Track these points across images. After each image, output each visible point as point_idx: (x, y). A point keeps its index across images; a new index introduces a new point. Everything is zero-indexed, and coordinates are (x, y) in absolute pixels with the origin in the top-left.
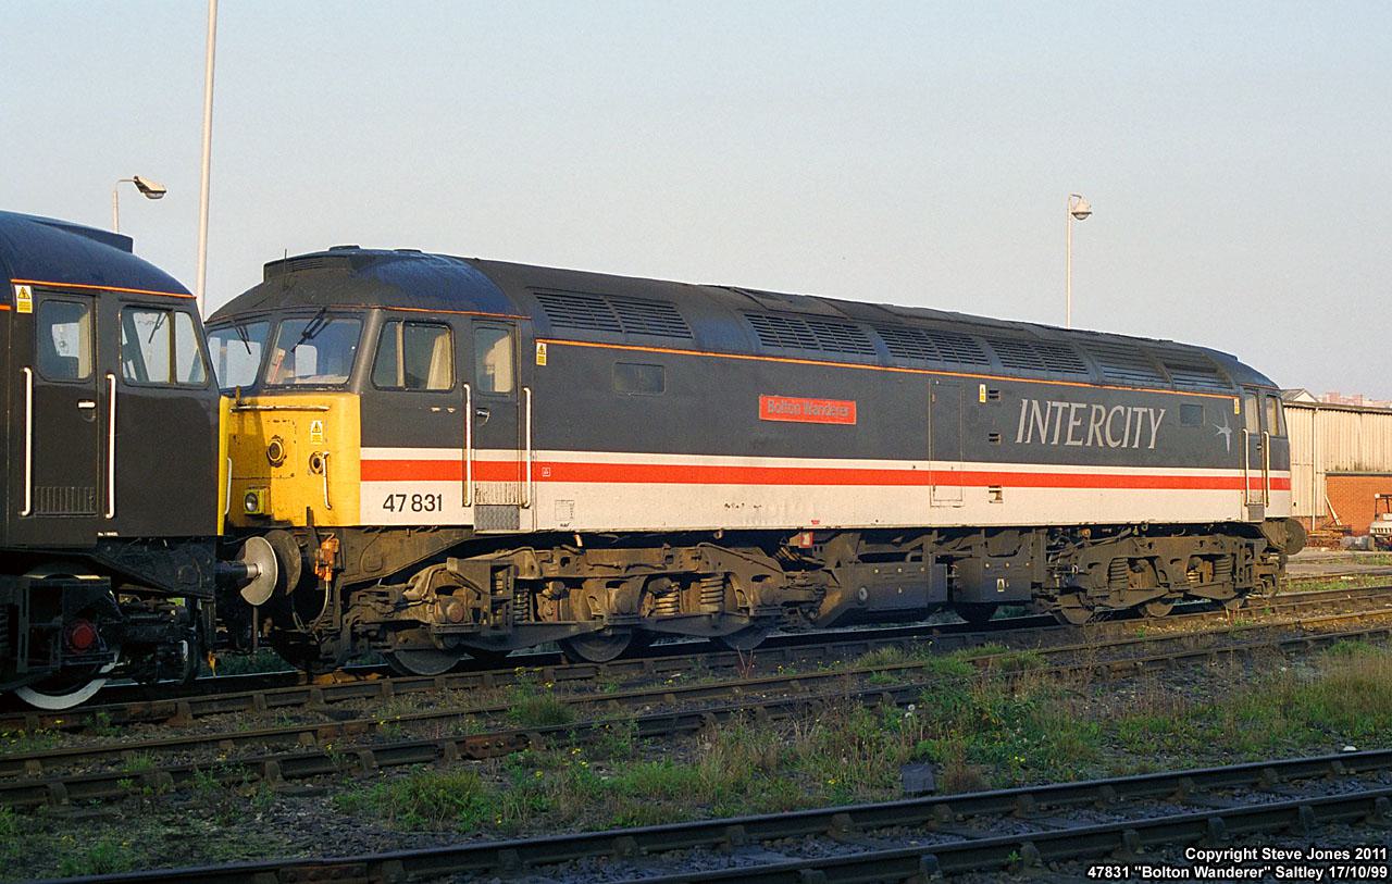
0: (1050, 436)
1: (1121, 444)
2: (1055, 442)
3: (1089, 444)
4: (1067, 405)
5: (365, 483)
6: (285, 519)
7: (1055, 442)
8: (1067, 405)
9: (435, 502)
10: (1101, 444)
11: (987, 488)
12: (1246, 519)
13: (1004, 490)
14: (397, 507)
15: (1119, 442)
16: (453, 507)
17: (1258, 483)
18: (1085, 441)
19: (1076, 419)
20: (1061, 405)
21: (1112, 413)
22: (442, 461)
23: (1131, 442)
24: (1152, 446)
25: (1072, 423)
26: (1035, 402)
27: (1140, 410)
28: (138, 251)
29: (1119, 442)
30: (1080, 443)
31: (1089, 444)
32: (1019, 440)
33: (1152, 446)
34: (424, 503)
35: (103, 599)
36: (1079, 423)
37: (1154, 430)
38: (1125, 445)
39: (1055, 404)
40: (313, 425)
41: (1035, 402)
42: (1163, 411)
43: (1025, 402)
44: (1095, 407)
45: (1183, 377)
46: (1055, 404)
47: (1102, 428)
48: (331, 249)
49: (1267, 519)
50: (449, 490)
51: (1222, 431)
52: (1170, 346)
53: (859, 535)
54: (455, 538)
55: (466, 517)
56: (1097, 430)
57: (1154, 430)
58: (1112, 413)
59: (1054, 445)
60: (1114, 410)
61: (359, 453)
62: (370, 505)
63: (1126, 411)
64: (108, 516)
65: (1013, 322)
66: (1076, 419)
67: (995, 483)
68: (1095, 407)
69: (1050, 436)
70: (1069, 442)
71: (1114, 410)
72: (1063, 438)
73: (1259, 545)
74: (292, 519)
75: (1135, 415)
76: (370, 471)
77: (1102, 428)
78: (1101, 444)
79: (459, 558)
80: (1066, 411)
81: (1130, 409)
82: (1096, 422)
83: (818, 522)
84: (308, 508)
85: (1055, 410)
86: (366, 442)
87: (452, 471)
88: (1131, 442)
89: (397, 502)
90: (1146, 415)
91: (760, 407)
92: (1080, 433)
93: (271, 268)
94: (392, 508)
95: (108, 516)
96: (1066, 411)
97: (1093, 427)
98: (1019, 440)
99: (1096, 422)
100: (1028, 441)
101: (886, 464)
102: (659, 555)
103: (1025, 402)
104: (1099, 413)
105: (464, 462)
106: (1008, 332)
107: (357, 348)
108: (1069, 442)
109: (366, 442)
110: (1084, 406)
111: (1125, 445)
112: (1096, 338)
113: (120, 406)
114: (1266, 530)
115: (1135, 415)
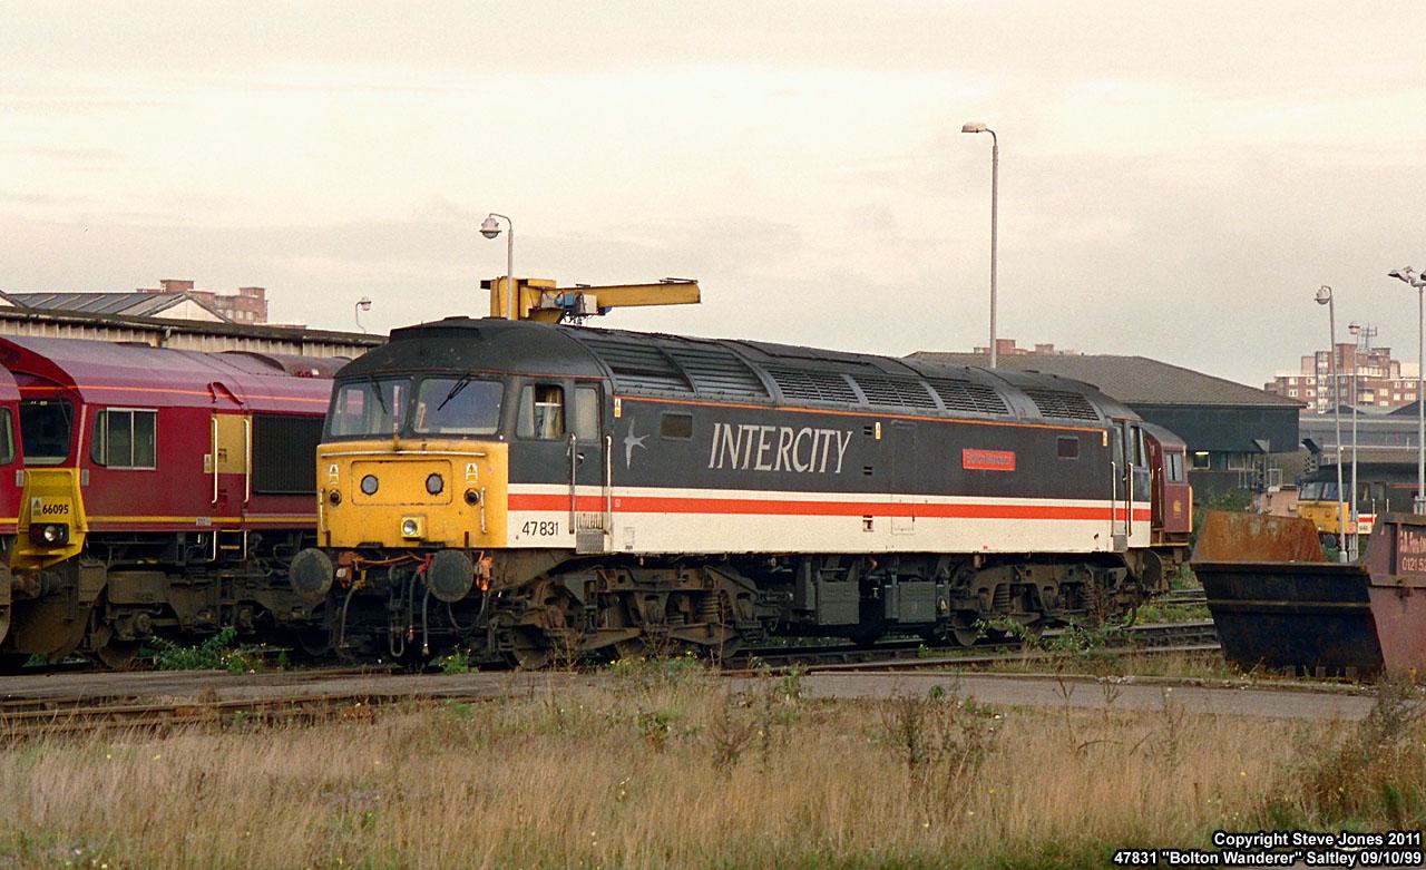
0: (741, 462)
1: (808, 468)
3: (777, 468)
4: (757, 428)
5: (513, 513)
6: (440, 540)
8: (757, 428)
10: (788, 469)
11: (862, 518)
12: (1111, 550)
13: (875, 519)
14: (531, 530)
15: (807, 466)
16: (561, 533)
17: (1109, 514)
18: (774, 467)
19: (765, 443)
20: (751, 428)
21: (799, 436)
22: (871, 504)
24: (838, 471)
25: (762, 447)
26: (727, 427)
27: (828, 433)
28: (1101, 390)
29: (807, 466)
30: (769, 468)
31: (777, 468)
32: (711, 465)
33: (838, 471)
34: (548, 528)
36: (767, 447)
37: (841, 453)
38: (811, 470)
39: (746, 427)
40: (468, 468)
41: (727, 427)
42: (850, 433)
43: (718, 426)
44: (783, 430)
45: (722, 379)
46: (746, 427)
47: (790, 452)
48: (446, 319)
49: (1130, 549)
50: (561, 518)
51: (638, 442)
52: (463, 324)
53: (838, 561)
54: (561, 558)
55: (569, 541)
56: (785, 453)
57: (841, 453)
58: (799, 436)
59: (838, 475)
60: (802, 433)
61: (506, 488)
62: (515, 530)
63: (814, 433)
65: (859, 355)
66: (765, 443)
67: (868, 512)
68: (783, 430)
69: (741, 462)
70: (759, 467)
71: (802, 433)
73: (1120, 573)
74: (384, 541)
75: (822, 437)
76: (516, 503)
77: (790, 452)
78: (788, 469)
80: (756, 434)
81: (817, 431)
82: (784, 446)
83: (631, 547)
84: (467, 534)
85: (745, 433)
87: (568, 503)
89: (532, 527)
92: (769, 457)
96: (756, 434)
97: (783, 450)
98: (711, 465)
99: (784, 446)
100: (720, 466)
101: (649, 492)
102: (1196, 558)
103: (718, 426)
104: (787, 435)
105: (1112, 509)
106: (801, 362)
107: (502, 406)
108: (759, 467)
110: (774, 429)
111: (811, 470)
112: (609, 338)
114: (1130, 561)
115: (822, 437)
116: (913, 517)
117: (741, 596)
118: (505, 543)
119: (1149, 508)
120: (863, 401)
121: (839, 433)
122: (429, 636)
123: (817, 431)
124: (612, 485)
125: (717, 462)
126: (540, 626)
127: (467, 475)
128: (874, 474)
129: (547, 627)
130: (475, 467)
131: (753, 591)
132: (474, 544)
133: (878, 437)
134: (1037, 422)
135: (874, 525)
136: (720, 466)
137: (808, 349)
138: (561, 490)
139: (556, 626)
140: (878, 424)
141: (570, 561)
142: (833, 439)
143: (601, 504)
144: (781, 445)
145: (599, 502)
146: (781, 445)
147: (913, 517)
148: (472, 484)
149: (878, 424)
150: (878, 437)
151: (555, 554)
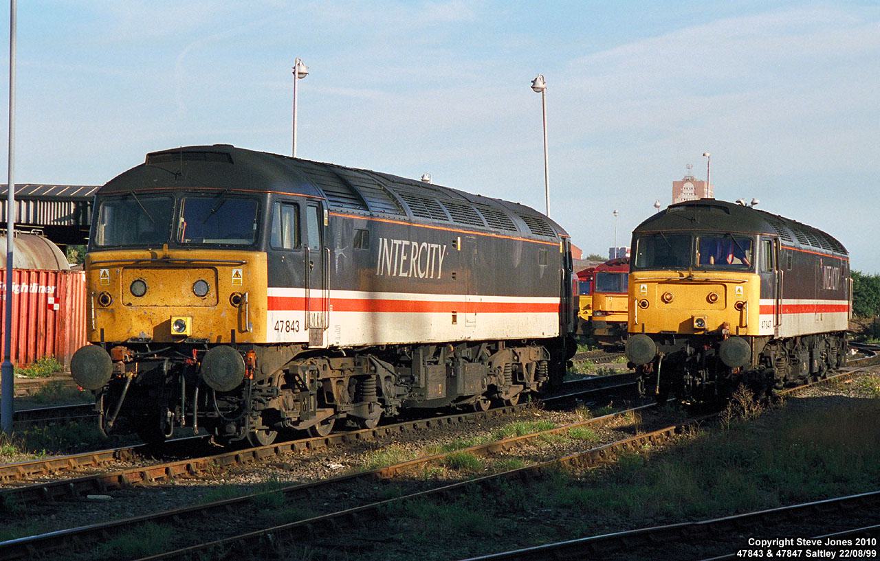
0: (392, 272)
1: (425, 276)
2: (394, 275)
3: (410, 276)
4: (407, 243)
5: (271, 311)
7: (394, 275)
9: (290, 327)
13: (458, 314)
18: (408, 275)
23: (430, 275)
24: (439, 278)
26: (386, 240)
31: (410, 276)
32: (378, 274)
33: (439, 278)
35: (691, 237)
38: (426, 277)
41: (386, 240)
42: (445, 246)
43: (381, 239)
50: (298, 316)
55: (303, 336)
64: (311, 410)
67: (454, 309)
69: (392, 272)
72: (398, 273)
75: (432, 249)
79: (631, 249)
86: (762, 297)
87: (306, 304)
88: (430, 275)
90: (437, 249)
91: (427, 226)
93: (149, 155)
94: (278, 329)
95: (311, 410)
96: (400, 246)
103: (381, 239)
108: (401, 274)
109: (762, 297)
111: (426, 277)
113: (290, 161)
115: (432, 249)
116: (476, 313)
117: (387, 378)
118: (265, 339)
119: (559, 302)
120: (451, 221)
121: (440, 246)
122: (198, 418)
123: (429, 245)
124: (332, 289)
125: (380, 273)
126: (278, 409)
127: (736, 293)
128: (457, 278)
129: (284, 410)
130: (241, 273)
131: (393, 374)
132: (107, 338)
133: (459, 249)
134: (529, 238)
135: (458, 319)
136: (431, 277)
137: (415, 181)
138: (299, 293)
139: (289, 409)
140: (459, 238)
141: (307, 353)
142: (437, 249)
143: (324, 305)
144: (412, 257)
145: (304, 300)
146: (412, 257)
147: (476, 313)
148: (742, 299)
149: (459, 238)
150: (459, 249)
151: (283, 349)
